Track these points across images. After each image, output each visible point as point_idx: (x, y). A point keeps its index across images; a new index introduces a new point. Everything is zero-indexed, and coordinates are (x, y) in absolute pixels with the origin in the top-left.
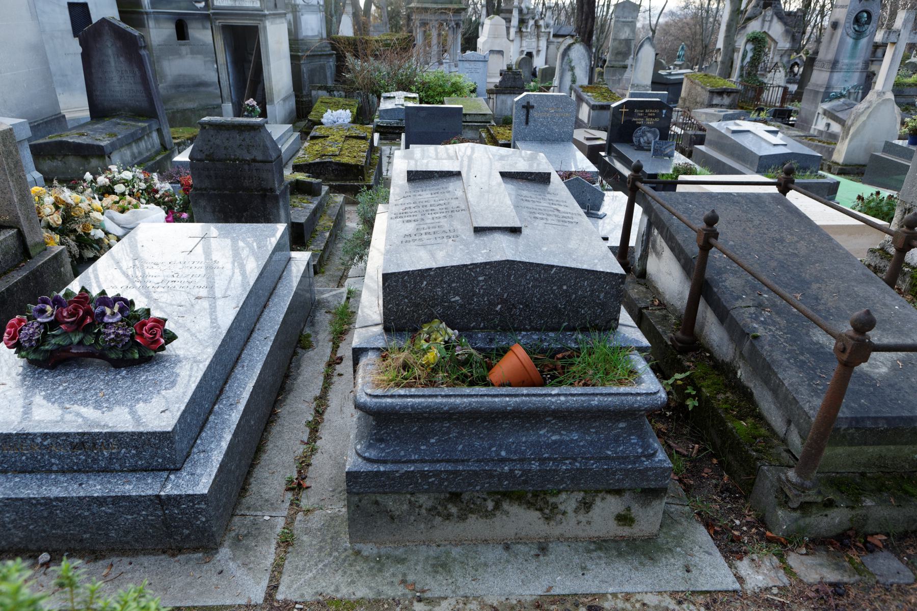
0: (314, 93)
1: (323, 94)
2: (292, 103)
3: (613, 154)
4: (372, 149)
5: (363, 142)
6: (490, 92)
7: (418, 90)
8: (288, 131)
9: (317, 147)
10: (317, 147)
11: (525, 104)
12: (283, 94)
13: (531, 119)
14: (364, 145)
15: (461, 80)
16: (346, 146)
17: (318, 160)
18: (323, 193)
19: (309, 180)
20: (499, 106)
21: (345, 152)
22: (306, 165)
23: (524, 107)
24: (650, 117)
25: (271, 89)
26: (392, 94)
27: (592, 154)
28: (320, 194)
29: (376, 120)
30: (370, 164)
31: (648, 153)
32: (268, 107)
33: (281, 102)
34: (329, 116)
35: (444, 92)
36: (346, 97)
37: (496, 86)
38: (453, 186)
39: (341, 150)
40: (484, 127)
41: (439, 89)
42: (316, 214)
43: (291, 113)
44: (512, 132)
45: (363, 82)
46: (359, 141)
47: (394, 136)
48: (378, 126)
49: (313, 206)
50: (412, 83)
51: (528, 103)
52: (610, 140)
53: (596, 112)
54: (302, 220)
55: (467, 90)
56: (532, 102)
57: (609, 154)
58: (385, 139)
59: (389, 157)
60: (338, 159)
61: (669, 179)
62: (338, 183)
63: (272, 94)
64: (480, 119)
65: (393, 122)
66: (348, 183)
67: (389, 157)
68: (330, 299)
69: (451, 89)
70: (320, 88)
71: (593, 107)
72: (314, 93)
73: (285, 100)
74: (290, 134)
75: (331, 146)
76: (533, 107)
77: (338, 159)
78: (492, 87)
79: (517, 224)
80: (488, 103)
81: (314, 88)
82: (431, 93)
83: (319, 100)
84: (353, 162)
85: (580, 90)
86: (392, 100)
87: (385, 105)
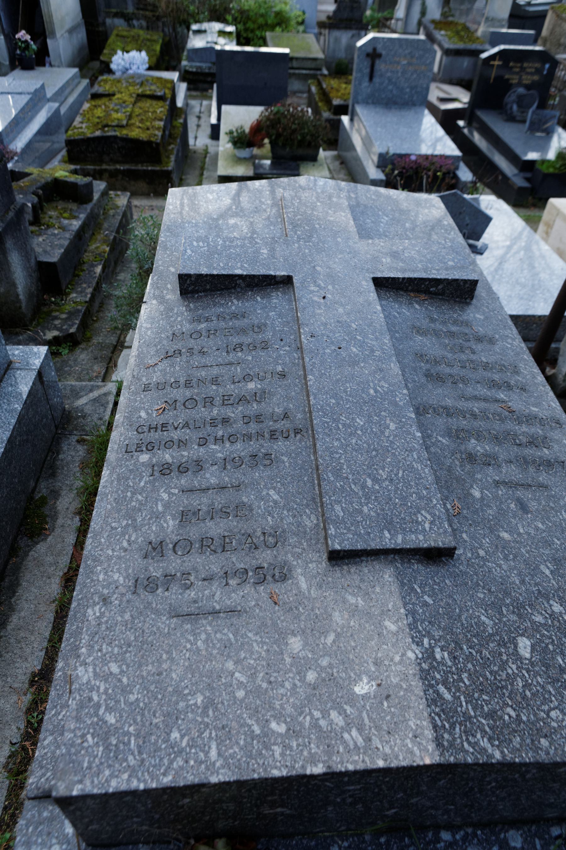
0: (109, 21)
1: (119, 22)
2: (81, 35)
3: (475, 124)
4: (174, 112)
5: (161, 103)
6: (321, 25)
7: (235, 22)
8: (72, 79)
9: (99, 112)
10: (99, 112)
11: (370, 50)
12: (68, 25)
13: (377, 74)
14: (161, 109)
15: (288, 8)
16: (137, 111)
17: (98, 133)
18: (96, 196)
19: (73, 178)
20: (331, 45)
21: (136, 121)
22: (83, 140)
23: (368, 55)
24: (528, 73)
25: (51, 16)
26: (205, 26)
27: (447, 121)
28: (91, 200)
29: (184, 63)
30: (170, 135)
31: (521, 126)
32: (49, 41)
33: (66, 35)
34: (119, 60)
35: (266, 24)
36: (148, 28)
37: (329, 18)
38: (266, 309)
39: (130, 117)
40: (314, 77)
41: (261, 21)
42: (80, 239)
43: (81, 49)
44: (351, 88)
45: (168, 7)
46: (154, 103)
47: (206, 86)
48: (187, 72)
49: (76, 224)
50: (227, 10)
51: (375, 49)
52: (474, 104)
53: (450, 58)
54: (54, 257)
55: (293, 23)
56: (380, 49)
57: (469, 124)
58: (195, 89)
59: (199, 118)
60: (125, 132)
61: (551, 170)
62: (127, 167)
63: (52, 23)
64: (309, 64)
65: (205, 66)
66: (140, 167)
67: (199, 118)
68: (88, 409)
69: (275, 21)
70: (116, 15)
71: (447, 52)
72: (109, 21)
73: (71, 31)
74: (76, 81)
75: (117, 111)
76: (380, 56)
77: (125, 132)
78: (323, 18)
79: (430, 533)
80: (318, 40)
81: (108, 15)
82: (250, 25)
83: (115, 32)
84: (144, 136)
85: (431, 27)
86: (203, 36)
87: (197, 42)
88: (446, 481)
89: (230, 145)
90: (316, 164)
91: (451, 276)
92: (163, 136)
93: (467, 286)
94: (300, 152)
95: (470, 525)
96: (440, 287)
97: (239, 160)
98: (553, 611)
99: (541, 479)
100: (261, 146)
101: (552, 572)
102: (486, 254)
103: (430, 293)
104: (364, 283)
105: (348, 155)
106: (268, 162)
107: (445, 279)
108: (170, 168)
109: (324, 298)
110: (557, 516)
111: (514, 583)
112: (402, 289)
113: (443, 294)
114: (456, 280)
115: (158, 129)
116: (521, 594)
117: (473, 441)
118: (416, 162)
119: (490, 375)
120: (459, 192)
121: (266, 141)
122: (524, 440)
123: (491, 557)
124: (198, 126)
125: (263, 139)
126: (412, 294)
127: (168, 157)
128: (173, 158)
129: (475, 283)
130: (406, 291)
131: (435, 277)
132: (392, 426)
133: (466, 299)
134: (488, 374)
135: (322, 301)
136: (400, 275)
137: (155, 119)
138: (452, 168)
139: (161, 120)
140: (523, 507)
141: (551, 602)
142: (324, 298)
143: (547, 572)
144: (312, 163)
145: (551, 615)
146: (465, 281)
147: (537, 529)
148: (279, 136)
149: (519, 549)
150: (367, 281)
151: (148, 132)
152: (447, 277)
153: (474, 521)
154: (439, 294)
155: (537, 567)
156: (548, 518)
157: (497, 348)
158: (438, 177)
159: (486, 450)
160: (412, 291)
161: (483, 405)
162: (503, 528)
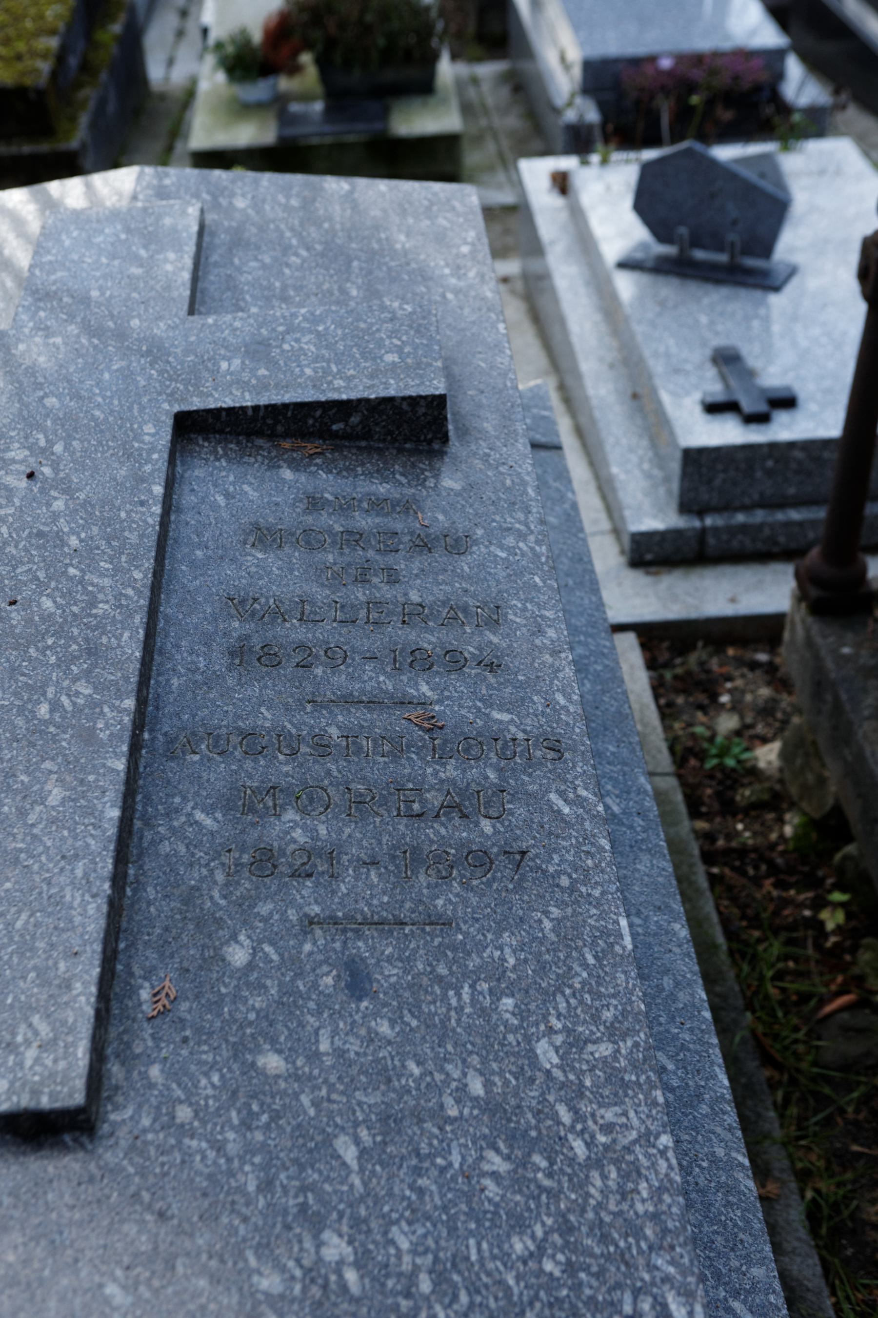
88: (167, 929)
89: (221, 77)
90: (432, 101)
91: (393, 388)
92: (54, 75)
93: (422, 410)
94: (389, 75)
95: (185, 1040)
96: (355, 419)
97: (244, 110)
98: (319, 1260)
99: (440, 902)
100: (294, 70)
101: (363, 1153)
102: (790, 289)
103: (335, 435)
104: (149, 428)
105: (524, 66)
106: (318, 107)
107: (360, 401)
108: (74, 144)
109: (31, 476)
110: (445, 998)
111: (241, 1190)
112: (260, 434)
113: (367, 435)
114: (390, 400)
115: (44, 56)
116: (245, 1220)
117: (290, 815)
118: (670, 73)
119: (413, 636)
120: (698, 146)
121: (306, 58)
122: (434, 799)
123: (204, 1123)
124: (180, 34)
125: (296, 53)
126: (287, 444)
127: (73, 119)
128: (84, 120)
129: (438, 402)
130: (272, 436)
131: (335, 396)
132: (56, 795)
133: (430, 442)
134: (411, 636)
135: (24, 483)
136: (248, 400)
137: (39, 33)
138: (764, 77)
139: (53, 32)
140: (357, 981)
141: (326, 1235)
142: (31, 476)
143: (350, 1154)
144: (417, 102)
145: (307, 1271)
146: (414, 401)
147: (372, 1037)
148: (330, 44)
149: (296, 1096)
150: (157, 422)
151: (20, 66)
152: (365, 395)
153: (199, 1031)
154: (358, 438)
155: (328, 1141)
156: (415, 1009)
157: (465, 565)
158: (692, 109)
159: (316, 838)
160: (286, 435)
161: (359, 716)
162: (273, 1041)
